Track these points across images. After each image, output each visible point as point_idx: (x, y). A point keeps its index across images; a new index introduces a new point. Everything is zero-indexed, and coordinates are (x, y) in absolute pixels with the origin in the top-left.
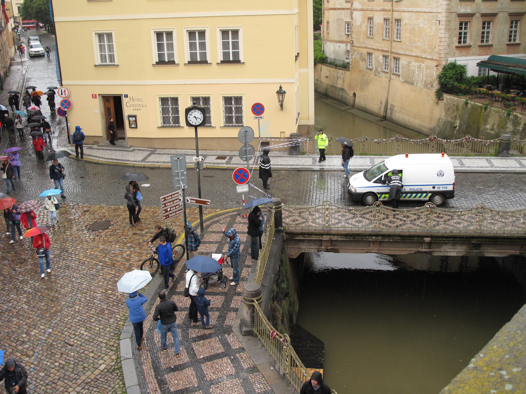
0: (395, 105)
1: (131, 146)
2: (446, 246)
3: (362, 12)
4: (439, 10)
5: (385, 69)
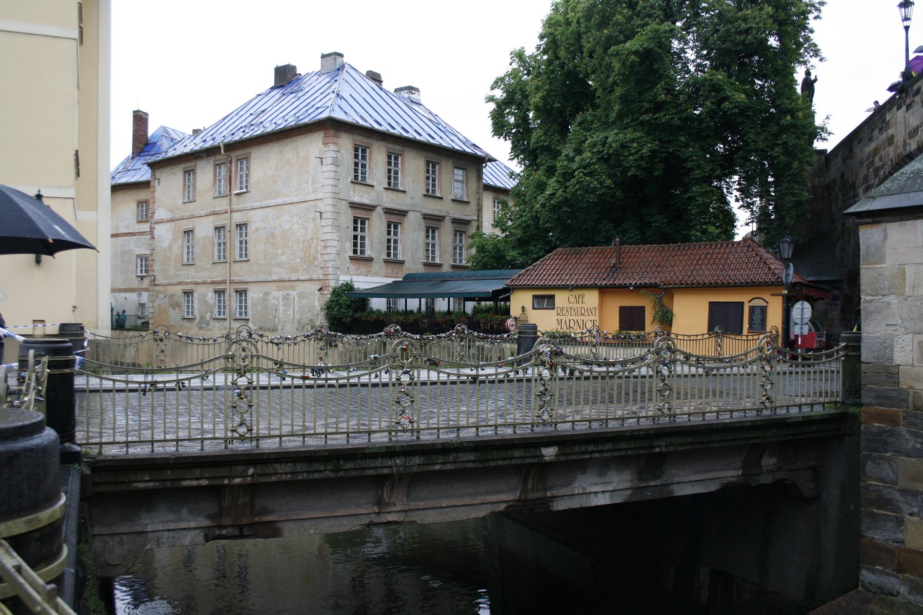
2: (583, 478)
3: (173, 224)
4: (319, 196)
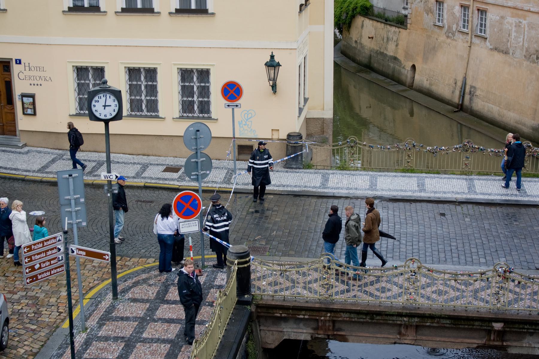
0: (477, 87)
1: (25, 145)
2: (531, 338)
5: (464, 27)
